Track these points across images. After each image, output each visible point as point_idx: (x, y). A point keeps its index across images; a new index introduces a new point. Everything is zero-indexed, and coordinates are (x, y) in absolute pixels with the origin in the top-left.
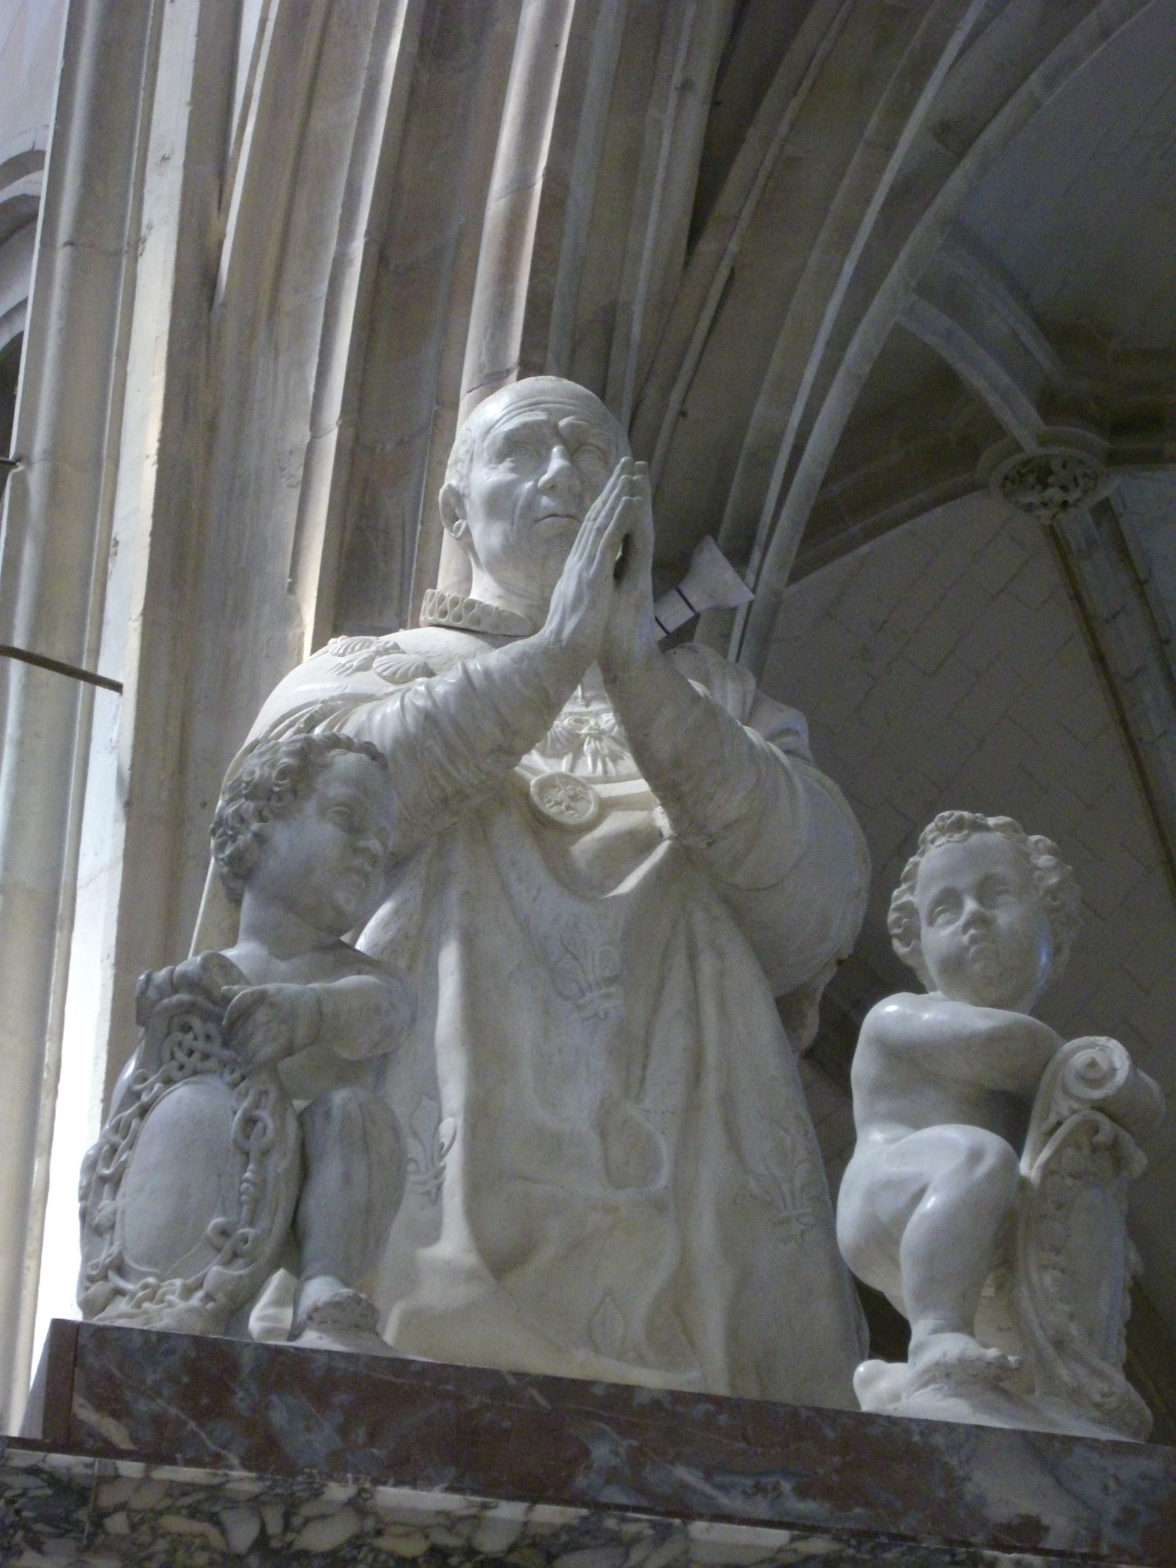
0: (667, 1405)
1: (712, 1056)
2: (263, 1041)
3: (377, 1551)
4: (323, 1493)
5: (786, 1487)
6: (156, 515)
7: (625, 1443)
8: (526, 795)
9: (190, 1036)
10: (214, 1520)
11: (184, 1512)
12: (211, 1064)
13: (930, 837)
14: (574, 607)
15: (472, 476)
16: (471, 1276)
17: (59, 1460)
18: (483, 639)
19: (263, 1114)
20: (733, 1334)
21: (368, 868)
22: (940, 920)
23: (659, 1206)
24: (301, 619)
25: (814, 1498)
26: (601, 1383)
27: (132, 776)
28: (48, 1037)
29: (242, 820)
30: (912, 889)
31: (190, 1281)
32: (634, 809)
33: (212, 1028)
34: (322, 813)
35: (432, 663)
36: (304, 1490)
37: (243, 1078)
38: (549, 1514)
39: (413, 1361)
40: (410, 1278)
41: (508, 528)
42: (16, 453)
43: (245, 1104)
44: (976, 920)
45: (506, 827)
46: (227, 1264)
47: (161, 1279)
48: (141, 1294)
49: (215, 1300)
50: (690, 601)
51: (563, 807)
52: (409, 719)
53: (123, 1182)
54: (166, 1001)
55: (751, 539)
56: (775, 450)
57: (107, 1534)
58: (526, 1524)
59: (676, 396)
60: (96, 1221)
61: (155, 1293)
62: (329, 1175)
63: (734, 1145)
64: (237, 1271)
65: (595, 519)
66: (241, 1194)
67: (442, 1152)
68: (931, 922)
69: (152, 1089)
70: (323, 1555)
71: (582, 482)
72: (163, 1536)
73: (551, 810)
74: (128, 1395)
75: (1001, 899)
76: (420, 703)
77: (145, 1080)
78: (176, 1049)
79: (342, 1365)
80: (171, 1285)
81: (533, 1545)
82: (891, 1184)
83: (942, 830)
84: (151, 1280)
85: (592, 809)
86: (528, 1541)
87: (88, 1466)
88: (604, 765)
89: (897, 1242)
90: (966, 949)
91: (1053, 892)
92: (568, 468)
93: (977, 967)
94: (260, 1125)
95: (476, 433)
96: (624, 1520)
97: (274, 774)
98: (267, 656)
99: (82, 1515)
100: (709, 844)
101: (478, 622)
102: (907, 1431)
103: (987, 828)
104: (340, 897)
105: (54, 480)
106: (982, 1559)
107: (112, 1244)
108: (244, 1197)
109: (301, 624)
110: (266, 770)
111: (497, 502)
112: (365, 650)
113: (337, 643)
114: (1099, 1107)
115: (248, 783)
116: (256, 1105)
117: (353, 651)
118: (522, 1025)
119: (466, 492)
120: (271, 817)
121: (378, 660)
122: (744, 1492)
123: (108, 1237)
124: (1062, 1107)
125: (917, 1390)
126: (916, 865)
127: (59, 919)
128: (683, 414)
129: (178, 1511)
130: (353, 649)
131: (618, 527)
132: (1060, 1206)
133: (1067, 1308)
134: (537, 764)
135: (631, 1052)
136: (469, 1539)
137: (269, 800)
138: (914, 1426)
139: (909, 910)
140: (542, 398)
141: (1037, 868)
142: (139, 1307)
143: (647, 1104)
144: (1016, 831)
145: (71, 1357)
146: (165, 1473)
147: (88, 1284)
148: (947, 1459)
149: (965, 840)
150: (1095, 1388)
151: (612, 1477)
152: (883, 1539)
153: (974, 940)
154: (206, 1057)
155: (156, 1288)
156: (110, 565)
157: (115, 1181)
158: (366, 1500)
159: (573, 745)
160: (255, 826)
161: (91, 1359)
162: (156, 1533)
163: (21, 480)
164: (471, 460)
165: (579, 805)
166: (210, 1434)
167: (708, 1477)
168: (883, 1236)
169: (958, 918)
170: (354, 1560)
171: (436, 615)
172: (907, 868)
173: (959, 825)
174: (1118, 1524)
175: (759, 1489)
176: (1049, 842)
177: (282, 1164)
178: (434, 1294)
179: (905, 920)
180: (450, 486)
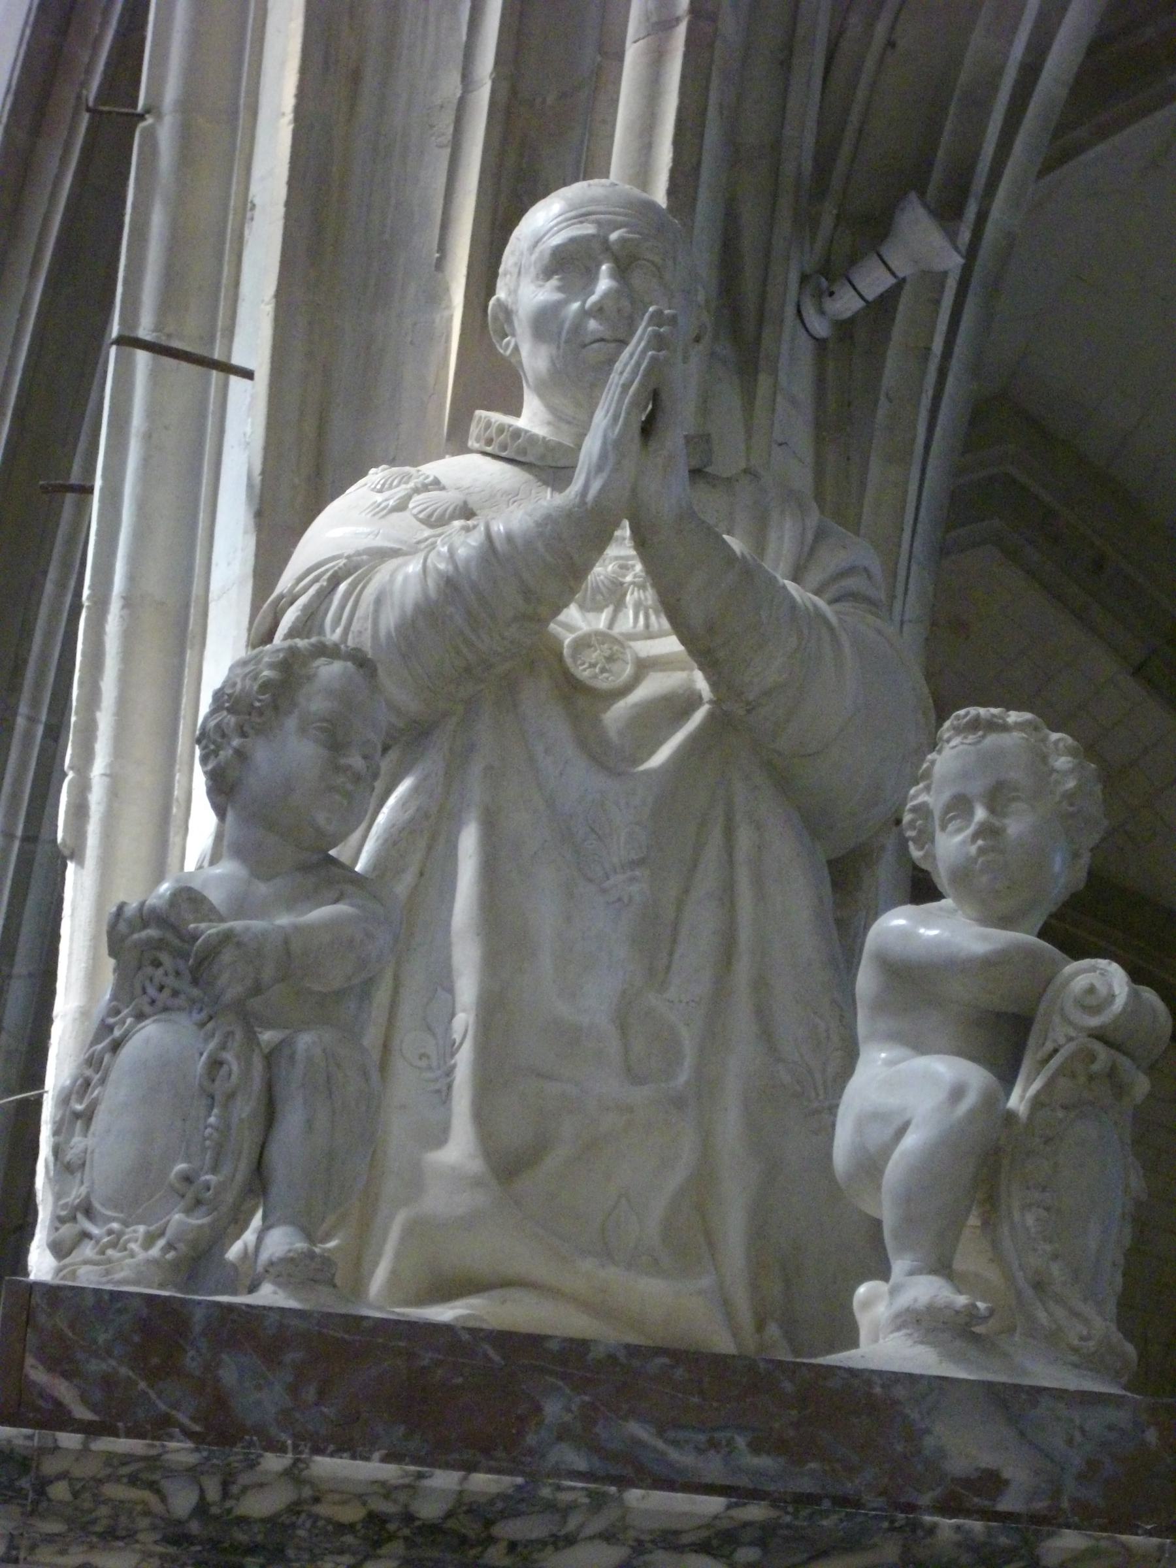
0: (623, 1360)
1: (745, 935)
2: (230, 982)
3: (316, 1518)
4: (259, 1464)
5: (741, 1442)
6: (291, 183)
7: (577, 1399)
8: (560, 657)
9: (160, 971)
10: (153, 1486)
11: (125, 1480)
12: (181, 1001)
13: (946, 736)
14: (600, 468)
15: (520, 292)
16: (477, 1183)
18: (530, 473)
19: (228, 1056)
20: (758, 1232)
21: (349, 787)
22: (950, 827)
23: (679, 1102)
24: (450, 300)
25: (768, 1453)
26: (556, 1337)
27: (263, 481)
28: (177, 767)
29: (224, 735)
30: (928, 789)
31: (152, 1228)
32: (674, 669)
33: (181, 964)
34: (303, 730)
35: (473, 502)
36: (240, 1461)
37: (211, 1018)
38: (483, 1482)
39: (367, 1318)
40: (416, 1182)
41: (554, 352)
42: (145, 105)
43: (212, 1045)
44: (987, 831)
45: (536, 696)
46: (188, 1211)
47: (126, 1224)
48: (105, 1240)
49: (175, 1249)
50: (893, 267)
51: (597, 670)
52: (431, 583)
53: (94, 1119)
54: (136, 936)
55: (964, 192)
56: (995, 88)
57: (49, 1500)
58: (461, 1492)
59: (881, 29)
60: (68, 1158)
61: (119, 1239)
62: (292, 1120)
63: (767, 1035)
64: (199, 1220)
65: (621, 373)
66: (205, 1139)
67: (452, 1049)
68: (943, 828)
69: (124, 1023)
70: (263, 1520)
71: (633, 303)
72: (105, 1502)
73: (583, 673)
74: (80, 1356)
75: (1014, 806)
76: (442, 566)
77: (118, 1012)
78: (147, 983)
79: (294, 1322)
80: (135, 1231)
81: (469, 1511)
82: (878, 1116)
83: (958, 730)
84: (115, 1226)
85: (629, 670)
86: (465, 1508)
87: (30, 1438)
88: (647, 618)
89: (881, 1172)
90: (974, 860)
91: (1070, 796)
92: (617, 291)
93: (984, 879)
94: (225, 1068)
95: (525, 245)
96: (559, 1488)
97: (256, 687)
98: (412, 343)
99: (25, 1483)
100: (749, 711)
101: (524, 452)
102: (869, 1383)
103: (1005, 728)
104: (321, 818)
105: (186, 136)
106: (921, 1525)
107: (82, 1183)
108: (208, 1143)
109: (449, 307)
110: (248, 682)
111: (545, 323)
112: (403, 486)
114: (1099, 1035)
115: (230, 696)
116: (223, 1046)
117: (390, 488)
118: (544, 914)
119: (514, 308)
120: (251, 732)
121: (417, 498)
122: (696, 1447)
123: (79, 1175)
125: (892, 1332)
126: (933, 762)
127: (190, 636)
128: (891, 44)
129: (118, 1480)
130: (391, 484)
131: (642, 384)
132: (1048, 1141)
133: (1048, 1248)
134: (575, 621)
135: (656, 940)
136: (406, 1506)
137: (250, 714)
138: (875, 1378)
139: (923, 811)
140: (590, 209)
141: (1053, 771)
142: (103, 1253)
143: (672, 993)
144: (1036, 729)
145: (24, 1317)
146: (105, 1444)
147: (57, 1224)
148: (907, 1411)
149: (979, 742)
150: (1074, 1331)
151: (563, 1434)
152: (826, 1504)
153: (981, 851)
154: (175, 993)
155: (120, 1235)
156: (246, 232)
157: (87, 1117)
158: (301, 1470)
159: (615, 595)
160: (236, 742)
161: (42, 1319)
162: (98, 1500)
163: (150, 136)
164: (519, 273)
165: (615, 667)
166: (160, 1395)
167: (661, 1433)
168: (871, 1166)
169: (968, 827)
170: (293, 1526)
171: (483, 442)
172: (925, 766)
173: (975, 725)
174: (1081, 1477)
175: (713, 1444)
176: (1070, 740)
177: (245, 1108)
178: (438, 1201)
179: (919, 822)
180: (498, 300)
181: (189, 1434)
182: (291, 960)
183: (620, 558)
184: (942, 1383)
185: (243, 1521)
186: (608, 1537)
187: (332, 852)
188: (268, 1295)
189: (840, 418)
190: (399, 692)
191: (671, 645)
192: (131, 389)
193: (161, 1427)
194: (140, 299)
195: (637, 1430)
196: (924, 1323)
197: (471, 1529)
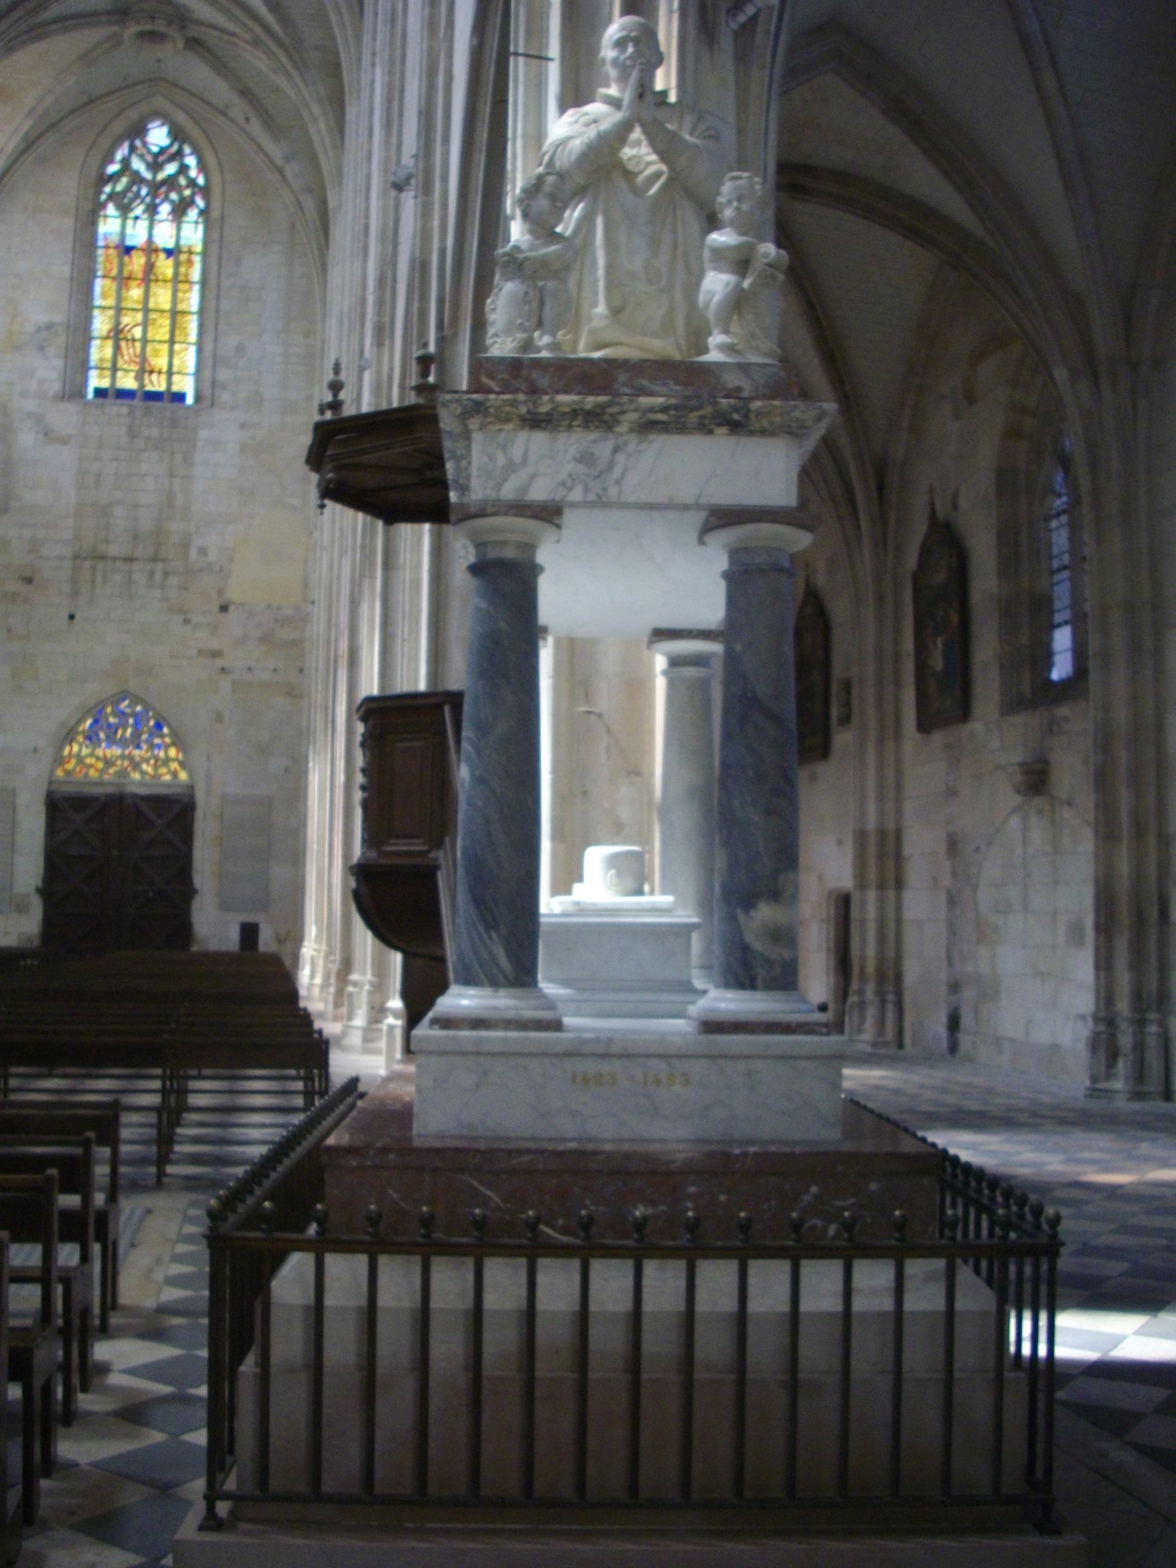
17: (475, 396)
82: (709, 292)
111: (615, 62)
113: (570, 112)
114: (769, 265)
124: (758, 265)
134: (627, 152)
135: (654, 244)
139: (720, 203)
151: (624, 384)
159: (638, 143)
168: (707, 304)
177: (535, 304)
178: (597, 323)
181: (524, 392)
182: (544, 262)
183: (637, 134)
184: (725, 364)
185: (540, 414)
186: (635, 410)
187: (558, 229)
188: (544, 354)
189: (742, 57)
190: (579, 180)
191: (654, 157)
192: (519, 68)
193: (516, 391)
194: (519, 42)
195: (644, 382)
196: (723, 348)
197: (599, 410)
